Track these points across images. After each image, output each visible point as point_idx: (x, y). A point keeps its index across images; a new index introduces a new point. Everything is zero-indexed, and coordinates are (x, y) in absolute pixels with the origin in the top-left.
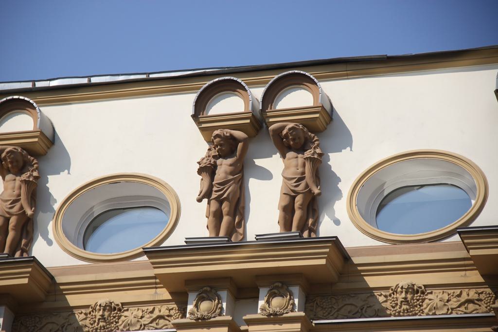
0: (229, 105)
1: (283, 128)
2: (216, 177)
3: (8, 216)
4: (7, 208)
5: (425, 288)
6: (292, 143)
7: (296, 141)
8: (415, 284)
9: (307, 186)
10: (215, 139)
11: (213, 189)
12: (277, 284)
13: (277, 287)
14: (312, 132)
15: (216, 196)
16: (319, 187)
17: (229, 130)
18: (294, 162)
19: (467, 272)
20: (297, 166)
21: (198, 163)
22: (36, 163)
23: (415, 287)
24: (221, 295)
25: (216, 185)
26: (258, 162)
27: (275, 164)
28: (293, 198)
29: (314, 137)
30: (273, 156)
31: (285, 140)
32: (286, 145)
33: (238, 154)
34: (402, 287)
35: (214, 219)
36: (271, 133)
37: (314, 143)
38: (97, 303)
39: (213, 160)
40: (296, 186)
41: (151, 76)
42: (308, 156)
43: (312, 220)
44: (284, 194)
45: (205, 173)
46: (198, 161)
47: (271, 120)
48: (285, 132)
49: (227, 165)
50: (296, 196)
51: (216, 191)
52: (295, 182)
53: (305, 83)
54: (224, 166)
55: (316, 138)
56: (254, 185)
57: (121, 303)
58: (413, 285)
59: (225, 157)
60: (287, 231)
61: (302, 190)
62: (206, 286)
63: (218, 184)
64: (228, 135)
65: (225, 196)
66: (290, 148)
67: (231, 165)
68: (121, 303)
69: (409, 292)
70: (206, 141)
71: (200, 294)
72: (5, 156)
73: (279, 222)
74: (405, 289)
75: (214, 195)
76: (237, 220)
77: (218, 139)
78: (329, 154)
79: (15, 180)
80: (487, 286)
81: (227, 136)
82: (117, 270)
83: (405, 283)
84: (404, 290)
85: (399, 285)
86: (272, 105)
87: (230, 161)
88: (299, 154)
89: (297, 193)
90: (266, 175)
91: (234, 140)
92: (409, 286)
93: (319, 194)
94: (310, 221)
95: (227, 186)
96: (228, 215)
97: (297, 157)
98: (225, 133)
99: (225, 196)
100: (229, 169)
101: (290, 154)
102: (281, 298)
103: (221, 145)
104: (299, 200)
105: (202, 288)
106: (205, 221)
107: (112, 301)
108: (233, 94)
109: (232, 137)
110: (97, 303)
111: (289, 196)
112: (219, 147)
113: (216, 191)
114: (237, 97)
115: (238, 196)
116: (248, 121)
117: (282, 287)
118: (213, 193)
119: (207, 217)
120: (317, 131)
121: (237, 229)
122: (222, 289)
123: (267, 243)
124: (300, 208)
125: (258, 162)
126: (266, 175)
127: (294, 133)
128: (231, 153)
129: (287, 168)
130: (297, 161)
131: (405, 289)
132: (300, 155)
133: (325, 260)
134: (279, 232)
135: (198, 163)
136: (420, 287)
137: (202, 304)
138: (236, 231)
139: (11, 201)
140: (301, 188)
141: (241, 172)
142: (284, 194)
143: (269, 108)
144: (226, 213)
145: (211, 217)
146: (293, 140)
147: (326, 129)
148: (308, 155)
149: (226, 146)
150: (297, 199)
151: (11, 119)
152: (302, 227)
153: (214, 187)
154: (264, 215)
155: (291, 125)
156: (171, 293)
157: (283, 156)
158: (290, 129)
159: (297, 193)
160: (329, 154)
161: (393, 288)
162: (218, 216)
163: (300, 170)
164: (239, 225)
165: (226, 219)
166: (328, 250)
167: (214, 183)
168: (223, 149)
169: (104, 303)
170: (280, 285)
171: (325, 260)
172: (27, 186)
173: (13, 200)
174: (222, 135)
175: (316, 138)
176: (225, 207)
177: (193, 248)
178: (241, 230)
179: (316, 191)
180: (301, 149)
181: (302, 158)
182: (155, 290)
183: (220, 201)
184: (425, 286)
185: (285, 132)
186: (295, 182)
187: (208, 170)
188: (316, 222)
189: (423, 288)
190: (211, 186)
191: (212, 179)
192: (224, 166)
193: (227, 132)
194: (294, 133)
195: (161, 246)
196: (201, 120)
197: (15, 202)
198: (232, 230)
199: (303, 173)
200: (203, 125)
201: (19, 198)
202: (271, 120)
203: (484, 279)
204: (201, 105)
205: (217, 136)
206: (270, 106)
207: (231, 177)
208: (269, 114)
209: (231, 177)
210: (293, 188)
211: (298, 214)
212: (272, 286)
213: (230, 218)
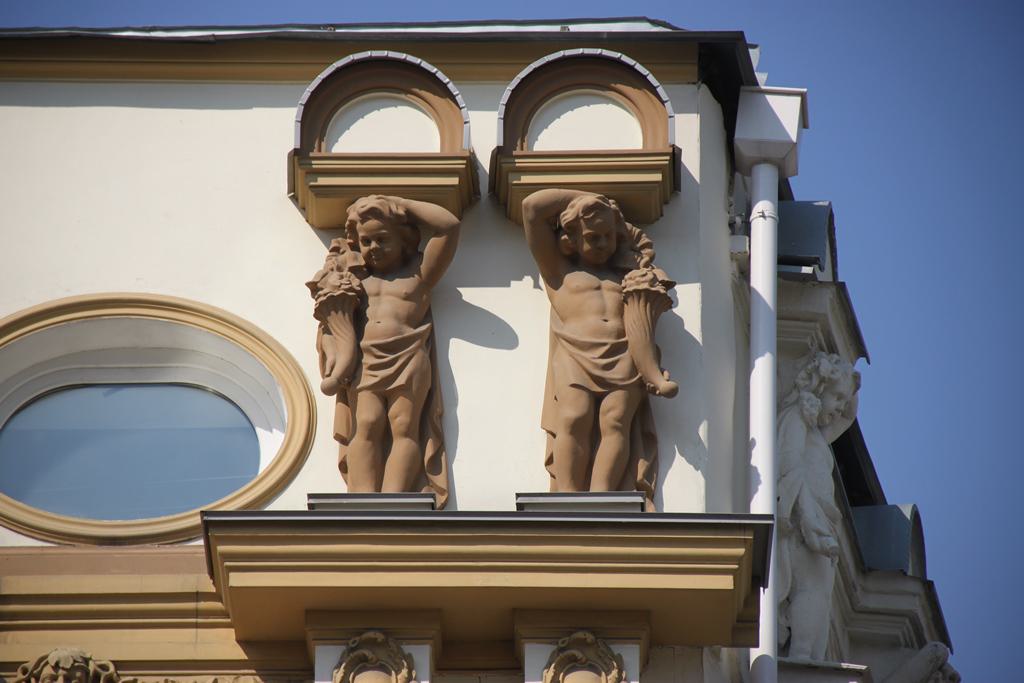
0: (389, 130)
1: (564, 204)
2: (369, 327)
3: (597, 389)
4: (596, 366)
5: (117, 668)
6: (586, 247)
7: (603, 243)
8: (90, 659)
9: (634, 369)
10: (362, 222)
11: (363, 361)
12: (371, 635)
13: (582, 644)
14: (635, 223)
15: (376, 380)
16: (666, 373)
17: (403, 200)
18: (592, 301)
19: (199, 630)
20: (603, 311)
21: (308, 284)
22: (648, 245)
23: (92, 667)
24: (416, 658)
25: (374, 350)
26: (471, 295)
27: (522, 303)
28: (596, 400)
29: (639, 237)
30: (513, 283)
31: (565, 237)
32: (567, 252)
33: (424, 267)
34: (57, 664)
35: (370, 443)
36: (527, 217)
37: (638, 251)
38: (46, 657)
39: (355, 282)
40: (609, 367)
41: (574, 28)
42: (641, 287)
43: (646, 463)
44: (573, 386)
45: (340, 313)
46: (310, 279)
47: (526, 179)
48: (568, 215)
49: (397, 296)
50: (608, 393)
51: (373, 368)
52: (603, 356)
53: (417, 90)
54: (387, 300)
55: (644, 240)
56: (462, 357)
57: (114, 662)
58: (86, 661)
59: (387, 272)
60: (579, 490)
61: (622, 380)
62: (582, 629)
63: (386, 348)
64: (401, 212)
65: (401, 380)
66: (575, 262)
67: (407, 297)
68: (113, 662)
69: (75, 678)
70: (312, 226)
71: (561, 650)
72: (577, 219)
73: (549, 461)
74: (63, 669)
75: (368, 379)
76: (429, 452)
77: (373, 223)
78: (460, 289)
79: (599, 288)
80: (254, 672)
81: (398, 216)
82: (135, 568)
83: (66, 653)
84: (61, 672)
85: (49, 659)
86: (523, 141)
87: (403, 285)
88: (603, 279)
89: (609, 386)
90: (496, 334)
91: (412, 229)
92: (75, 661)
93: (672, 393)
94: (642, 466)
95: (404, 354)
96: (406, 434)
97: (599, 288)
98: (394, 209)
99: (401, 380)
100: (405, 307)
101: (577, 279)
102: (595, 675)
103: (379, 239)
104: (613, 406)
105: (360, 633)
106: (540, 446)
107: (88, 656)
108: (603, 96)
109: (412, 221)
110: (46, 657)
111: (584, 393)
112: (374, 245)
113: (373, 368)
114: (420, 113)
115: (429, 387)
116: (454, 181)
117: (385, 643)
118: (365, 371)
119: (338, 437)
120: (644, 220)
121: (430, 476)
122: (418, 640)
123: (527, 521)
124: (615, 428)
125: (471, 295)
126: (496, 334)
127: (598, 221)
128: (398, 255)
129: (560, 315)
130: (602, 296)
131: (63, 669)
132: (607, 284)
133: (731, 577)
134: (548, 491)
135: (308, 284)
136: (104, 668)
137: (357, 677)
138: (428, 482)
139: (606, 348)
140: (617, 374)
141: (430, 319)
142: (573, 386)
143: (518, 148)
144: (403, 428)
145: (563, 437)
146: (593, 239)
147: (658, 219)
148: (638, 283)
149: (397, 246)
150: (606, 403)
151: (393, 108)
152: (621, 479)
153: (365, 355)
154: (503, 435)
155: (590, 198)
156: (243, 642)
157: (555, 282)
158: (588, 209)
159: (609, 386)
160: (460, 289)
161: (30, 666)
162: (381, 437)
163: (613, 323)
164: (436, 464)
165: (401, 448)
166: (741, 551)
167: (364, 343)
168: (387, 250)
169: (67, 659)
170: (380, 637)
171: (731, 577)
172: (651, 306)
173: (613, 345)
174: (386, 212)
175: (644, 240)
176: (400, 413)
177: (324, 521)
178: (439, 480)
179: (663, 383)
180: (611, 264)
181: (614, 290)
182: (194, 630)
183: (384, 394)
184: (118, 664)
185: (568, 215)
186: (603, 356)
187: (341, 307)
188: (654, 473)
189: (112, 668)
190: (358, 353)
191: (359, 333)
192: (387, 300)
193: (398, 205)
194: (598, 221)
195: (267, 509)
196: (317, 164)
197: (618, 349)
198: (419, 476)
199: (621, 333)
200: (322, 181)
201: (623, 340)
202: (526, 179)
203: (247, 654)
204: (316, 122)
205: (372, 213)
206: (519, 143)
207: (410, 331)
208: (520, 163)
209: (410, 331)
210: (598, 373)
211: (609, 446)
212: (357, 639)
213: (413, 443)
